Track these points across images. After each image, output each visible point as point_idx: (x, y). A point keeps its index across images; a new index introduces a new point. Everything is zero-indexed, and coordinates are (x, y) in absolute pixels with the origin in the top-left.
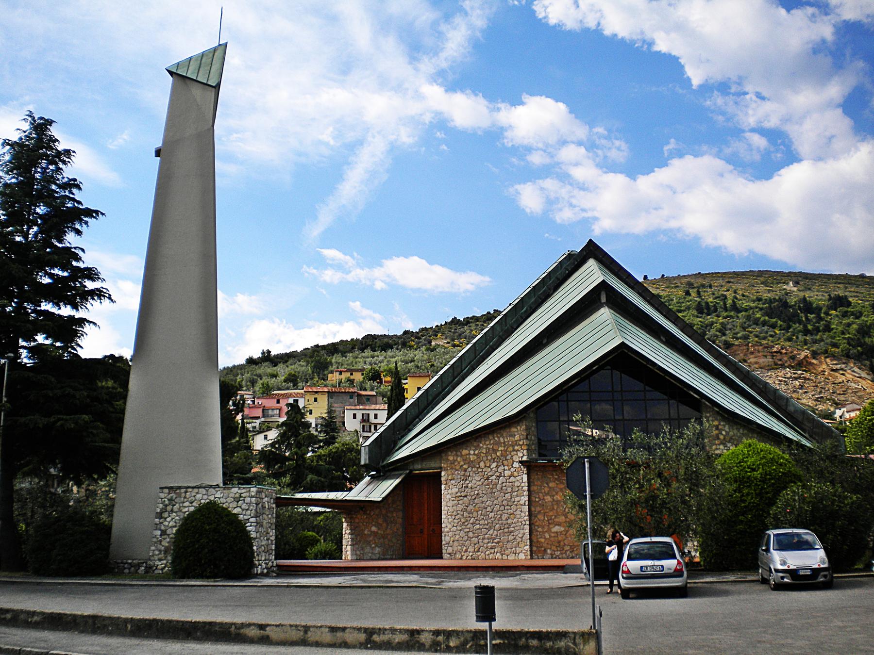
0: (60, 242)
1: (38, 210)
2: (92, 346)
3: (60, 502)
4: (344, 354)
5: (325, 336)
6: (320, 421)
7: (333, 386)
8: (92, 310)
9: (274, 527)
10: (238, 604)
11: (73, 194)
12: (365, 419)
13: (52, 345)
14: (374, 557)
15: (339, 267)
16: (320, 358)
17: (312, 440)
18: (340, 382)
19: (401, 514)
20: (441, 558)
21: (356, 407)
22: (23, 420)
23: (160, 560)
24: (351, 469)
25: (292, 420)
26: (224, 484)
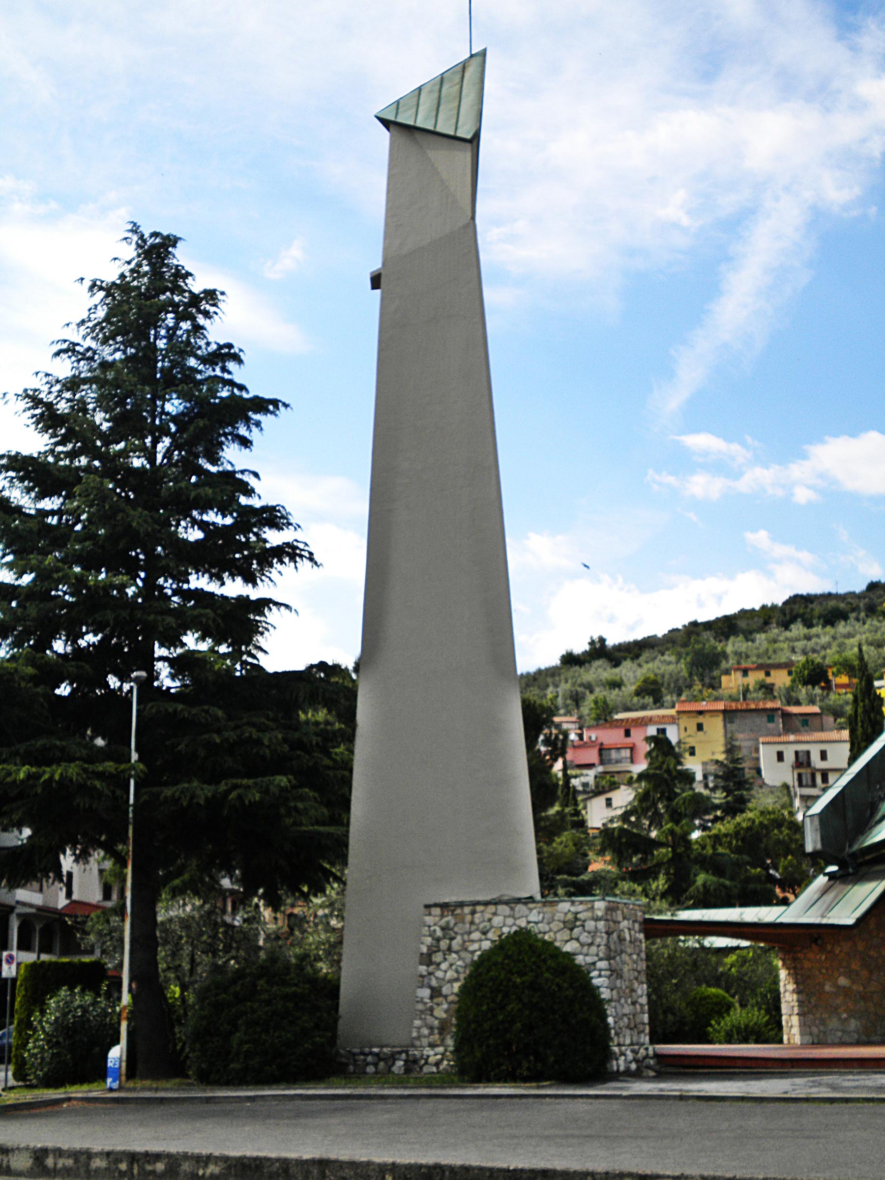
0: (215, 461)
1: (168, 407)
2: (283, 649)
3: (242, 939)
4: (748, 635)
5: (701, 604)
6: (712, 768)
7: (732, 698)
8: (280, 582)
9: (643, 978)
10: (588, 1132)
11: (230, 373)
12: (802, 761)
13: (212, 650)
14: (846, 1039)
15: (719, 467)
16: (702, 648)
17: (700, 806)
18: (746, 691)
21: (783, 738)
22: (168, 792)
23: (432, 1046)
24: (783, 862)
25: (660, 768)
26: (543, 896)
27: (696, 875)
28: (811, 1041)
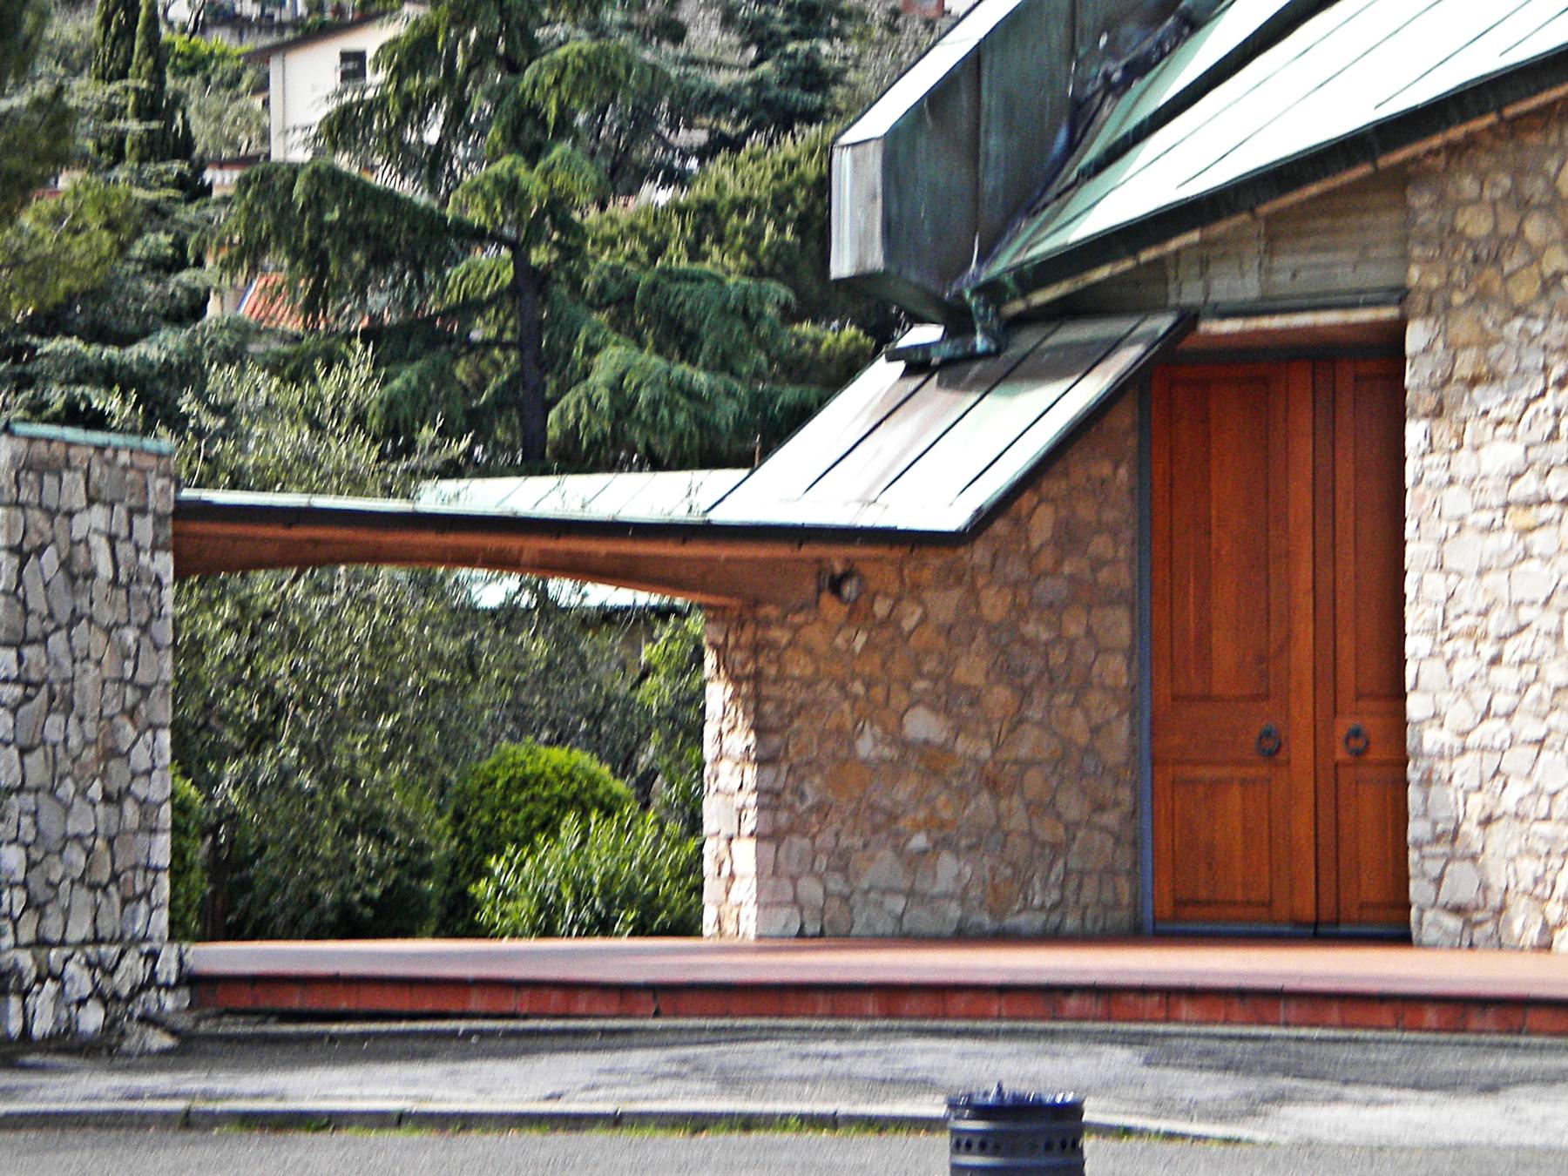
14: (920, 918)
19: (1118, 625)
20: (1401, 937)
27: (592, 351)
28: (795, 928)
